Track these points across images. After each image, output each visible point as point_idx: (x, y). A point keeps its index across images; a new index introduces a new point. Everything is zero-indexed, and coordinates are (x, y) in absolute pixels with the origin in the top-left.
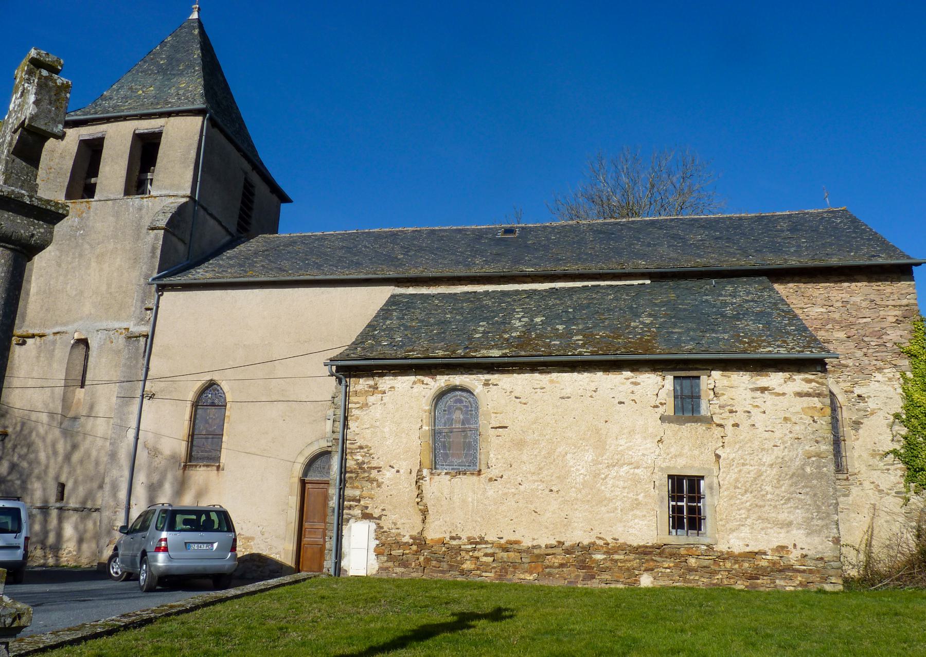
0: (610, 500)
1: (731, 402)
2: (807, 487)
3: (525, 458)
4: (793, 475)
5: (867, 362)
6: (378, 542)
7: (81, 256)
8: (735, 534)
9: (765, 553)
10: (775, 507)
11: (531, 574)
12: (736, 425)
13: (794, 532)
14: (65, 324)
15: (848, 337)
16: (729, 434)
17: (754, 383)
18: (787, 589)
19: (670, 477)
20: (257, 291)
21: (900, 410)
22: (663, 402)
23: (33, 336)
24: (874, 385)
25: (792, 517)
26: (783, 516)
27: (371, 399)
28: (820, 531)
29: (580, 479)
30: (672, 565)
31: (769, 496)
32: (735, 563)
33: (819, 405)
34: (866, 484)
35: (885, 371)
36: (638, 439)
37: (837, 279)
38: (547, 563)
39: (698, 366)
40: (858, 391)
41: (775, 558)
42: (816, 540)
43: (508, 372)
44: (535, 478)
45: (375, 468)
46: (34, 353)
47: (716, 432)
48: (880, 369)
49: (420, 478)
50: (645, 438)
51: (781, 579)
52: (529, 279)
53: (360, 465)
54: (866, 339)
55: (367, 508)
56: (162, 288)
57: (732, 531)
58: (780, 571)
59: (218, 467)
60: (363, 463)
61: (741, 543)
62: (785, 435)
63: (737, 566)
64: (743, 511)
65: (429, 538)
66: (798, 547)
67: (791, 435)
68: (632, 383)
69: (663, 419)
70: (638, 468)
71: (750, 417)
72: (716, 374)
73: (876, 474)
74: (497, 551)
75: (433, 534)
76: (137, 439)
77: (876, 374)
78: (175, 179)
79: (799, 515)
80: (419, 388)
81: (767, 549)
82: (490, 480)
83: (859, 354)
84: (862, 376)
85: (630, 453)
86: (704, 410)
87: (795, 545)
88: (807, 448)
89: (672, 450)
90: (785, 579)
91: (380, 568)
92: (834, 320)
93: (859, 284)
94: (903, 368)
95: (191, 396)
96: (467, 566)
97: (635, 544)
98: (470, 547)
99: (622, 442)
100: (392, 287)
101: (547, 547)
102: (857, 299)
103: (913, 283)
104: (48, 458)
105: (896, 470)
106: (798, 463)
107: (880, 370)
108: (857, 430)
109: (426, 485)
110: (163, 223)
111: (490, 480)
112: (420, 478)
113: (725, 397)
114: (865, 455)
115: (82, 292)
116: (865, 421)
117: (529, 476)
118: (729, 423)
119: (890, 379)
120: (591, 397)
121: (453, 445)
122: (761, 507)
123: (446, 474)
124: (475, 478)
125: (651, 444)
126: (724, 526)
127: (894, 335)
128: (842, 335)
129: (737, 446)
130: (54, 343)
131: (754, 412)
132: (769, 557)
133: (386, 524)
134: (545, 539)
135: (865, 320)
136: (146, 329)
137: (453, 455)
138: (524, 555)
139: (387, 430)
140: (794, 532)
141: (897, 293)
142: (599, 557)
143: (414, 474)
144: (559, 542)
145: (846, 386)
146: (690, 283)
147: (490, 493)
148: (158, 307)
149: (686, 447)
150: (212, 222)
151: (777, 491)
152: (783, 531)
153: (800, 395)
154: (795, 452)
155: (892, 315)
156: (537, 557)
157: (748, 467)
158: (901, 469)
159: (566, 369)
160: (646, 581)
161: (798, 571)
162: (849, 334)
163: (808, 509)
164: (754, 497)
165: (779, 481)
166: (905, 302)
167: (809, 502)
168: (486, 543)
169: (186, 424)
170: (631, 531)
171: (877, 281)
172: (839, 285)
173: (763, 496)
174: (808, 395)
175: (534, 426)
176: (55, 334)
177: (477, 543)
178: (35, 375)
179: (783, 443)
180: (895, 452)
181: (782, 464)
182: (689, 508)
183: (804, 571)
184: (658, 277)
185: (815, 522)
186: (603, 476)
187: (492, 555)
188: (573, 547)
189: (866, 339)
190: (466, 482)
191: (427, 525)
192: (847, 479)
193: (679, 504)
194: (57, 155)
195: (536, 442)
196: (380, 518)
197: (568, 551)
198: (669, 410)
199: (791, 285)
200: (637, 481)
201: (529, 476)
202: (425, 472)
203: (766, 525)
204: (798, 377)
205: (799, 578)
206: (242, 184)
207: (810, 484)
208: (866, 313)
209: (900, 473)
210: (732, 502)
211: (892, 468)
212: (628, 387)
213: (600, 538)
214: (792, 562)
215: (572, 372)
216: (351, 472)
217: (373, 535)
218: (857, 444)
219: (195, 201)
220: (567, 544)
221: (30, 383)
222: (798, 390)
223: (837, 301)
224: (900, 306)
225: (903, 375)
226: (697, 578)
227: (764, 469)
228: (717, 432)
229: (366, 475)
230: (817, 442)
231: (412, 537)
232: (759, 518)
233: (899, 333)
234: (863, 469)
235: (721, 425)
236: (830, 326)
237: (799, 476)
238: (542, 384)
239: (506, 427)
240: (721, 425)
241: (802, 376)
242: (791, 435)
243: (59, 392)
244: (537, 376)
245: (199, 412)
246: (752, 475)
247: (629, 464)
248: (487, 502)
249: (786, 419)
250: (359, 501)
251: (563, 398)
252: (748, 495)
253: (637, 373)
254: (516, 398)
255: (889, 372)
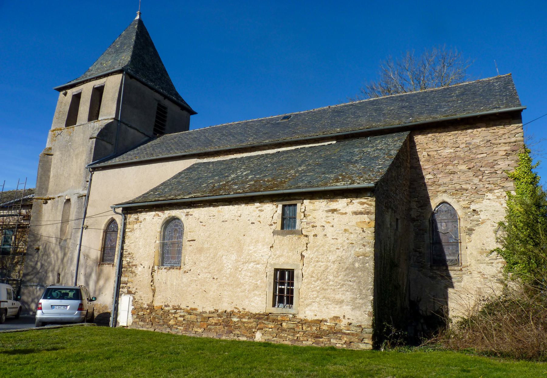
0: (243, 284)
1: (314, 220)
2: (354, 276)
3: (202, 259)
4: (347, 268)
5: (482, 186)
6: (133, 307)
7: (69, 155)
8: (309, 308)
9: (326, 321)
10: (334, 290)
11: (201, 328)
12: (315, 235)
13: (344, 307)
14: (63, 192)
15: (470, 169)
16: (311, 242)
17: (328, 207)
18: (337, 345)
19: (276, 270)
20: (133, 168)
21: (504, 219)
22: (275, 221)
23: (50, 199)
24: (486, 202)
25: (344, 297)
26: (338, 297)
27: (136, 226)
28: (361, 307)
29: (228, 271)
30: (273, 326)
31: (331, 283)
32: (308, 327)
33: (367, 220)
34: (475, 274)
35: (496, 191)
36: (260, 246)
37: (463, 127)
38: (209, 322)
39: (297, 198)
40: (473, 207)
41: (332, 324)
42: (358, 313)
43: (198, 207)
44: (206, 271)
45: (134, 265)
46: (50, 208)
47: (303, 240)
48: (491, 190)
49: (153, 271)
50: (263, 245)
51: (334, 339)
52: (267, 147)
53: (128, 263)
54: (482, 169)
55: (130, 287)
56: (95, 169)
57: (308, 305)
58: (334, 333)
59: (113, 265)
60: (130, 262)
61: (313, 314)
62: (344, 241)
63: (309, 329)
64: (315, 293)
65: (155, 305)
66: (346, 318)
67: (348, 241)
68: (260, 210)
69: (275, 233)
70: (258, 264)
71: (324, 230)
72: (306, 202)
73: (482, 266)
74: (186, 314)
75: (157, 304)
76: (80, 250)
77: (488, 194)
78: (109, 111)
79: (349, 296)
80: (156, 218)
81: (327, 318)
82: (185, 272)
83: (476, 180)
84: (477, 196)
85: (255, 255)
86: (298, 227)
87: (344, 316)
88: (357, 250)
89: (278, 252)
90: (337, 339)
91: (133, 322)
92: (460, 157)
93: (479, 130)
94: (509, 189)
95: (103, 227)
96: (172, 322)
97: (254, 313)
98: (173, 311)
99: (251, 248)
100: (196, 159)
101: (210, 313)
102: (477, 141)
103: (521, 125)
104: (55, 261)
105: (498, 263)
106: (351, 260)
107: (491, 191)
108: (470, 235)
109: (155, 274)
110: (95, 135)
111: (185, 272)
112: (153, 271)
113: (311, 217)
114: (475, 253)
115: (70, 175)
116: (476, 228)
117: (203, 269)
118: (311, 235)
119: (498, 197)
120: (238, 220)
121: (170, 252)
122: (325, 290)
123: (165, 268)
124: (178, 271)
125: (266, 249)
126: (303, 302)
127: (503, 165)
128: (464, 167)
129: (315, 250)
130: (58, 201)
131: (327, 226)
132: (328, 324)
133: (137, 297)
134: (209, 308)
135: (482, 155)
136: (86, 192)
137: (172, 258)
138: (198, 317)
139: (141, 243)
140: (344, 307)
141: (512, 133)
142: (235, 319)
143: (151, 269)
144: (215, 310)
145: (464, 203)
146: (357, 142)
147: (184, 280)
148: (91, 180)
149: (286, 251)
150: (132, 131)
151: (336, 280)
152: (337, 306)
153: (356, 213)
154: (350, 253)
155: (502, 150)
156: (204, 318)
157: (320, 263)
158: (502, 262)
159: (227, 203)
160: (259, 337)
161: (345, 334)
162: (470, 167)
163: (354, 292)
164: (322, 283)
165: (338, 272)
166: (513, 139)
167: (355, 287)
168: (181, 309)
169: (100, 242)
170: (253, 304)
171: (493, 126)
172: (464, 131)
173: (328, 282)
174: (361, 213)
175: (208, 239)
176: (59, 197)
177: (177, 309)
178: (50, 219)
179: (343, 246)
180: (498, 250)
181: (341, 261)
182: (288, 289)
183: (349, 334)
184: (338, 138)
185: (358, 301)
186: (240, 269)
187: (183, 316)
188: (222, 313)
189: (482, 169)
190: (174, 272)
191: (155, 298)
192: (461, 270)
193: (283, 287)
194: (63, 104)
195: (208, 249)
196: (134, 294)
197: (219, 316)
198: (278, 227)
199: (430, 135)
200: (257, 273)
201: (203, 269)
202: (156, 268)
203: (328, 302)
204: (356, 201)
205: (345, 339)
206: (156, 108)
207: (357, 275)
208: (484, 150)
209: (501, 265)
210: (309, 286)
211: (496, 261)
212: (257, 213)
213: (236, 308)
214: (342, 327)
215: (229, 205)
216: (125, 268)
217: (131, 303)
218: (469, 245)
219: (118, 121)
220: (220, 311)
221: (49, 223)
222: (355, 210)
223: (463, 143)
224: (510, 143)
225: (509, 193)
226: (286, 335)
227: (329, 264)
228: (304, 240)
229: (130, 269)
230: (364, 246)
231: (148, 305)
232: (324, 297)
233: (507, 162)
234: (473, 262)
235: (306, 236)
236: (456, 162)
237: (351, 269)
238: (214, 213)
239: (194, 240)
240: (306, 236)
241: (359, 200)
242: (348, 241)
243: (59, 225)
244: (211, 208)
245: (108, 235)
246: (322, 268)
247: (254, 262)
248: (182, 285)
249: (346, 230)
250: (127, 284)
251: (223, 221)
252: (319, 282)
253: (263, 204)
254: (201, 222)
255: (498, 192)
